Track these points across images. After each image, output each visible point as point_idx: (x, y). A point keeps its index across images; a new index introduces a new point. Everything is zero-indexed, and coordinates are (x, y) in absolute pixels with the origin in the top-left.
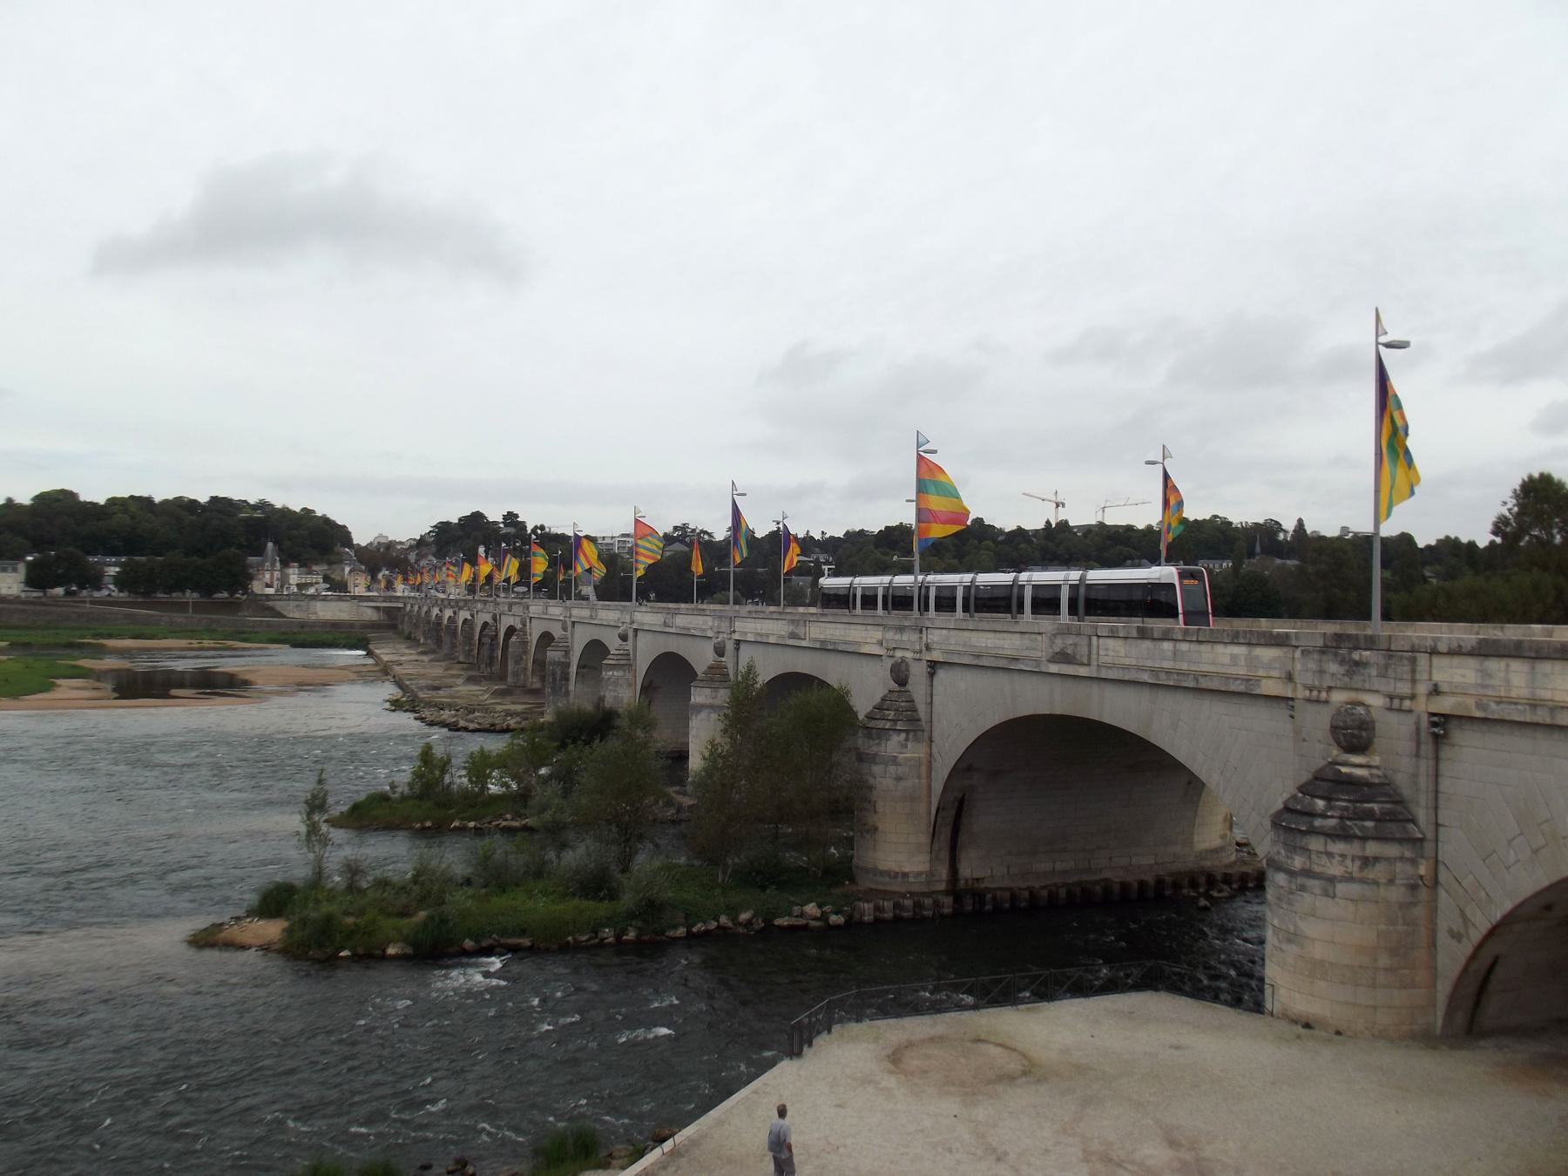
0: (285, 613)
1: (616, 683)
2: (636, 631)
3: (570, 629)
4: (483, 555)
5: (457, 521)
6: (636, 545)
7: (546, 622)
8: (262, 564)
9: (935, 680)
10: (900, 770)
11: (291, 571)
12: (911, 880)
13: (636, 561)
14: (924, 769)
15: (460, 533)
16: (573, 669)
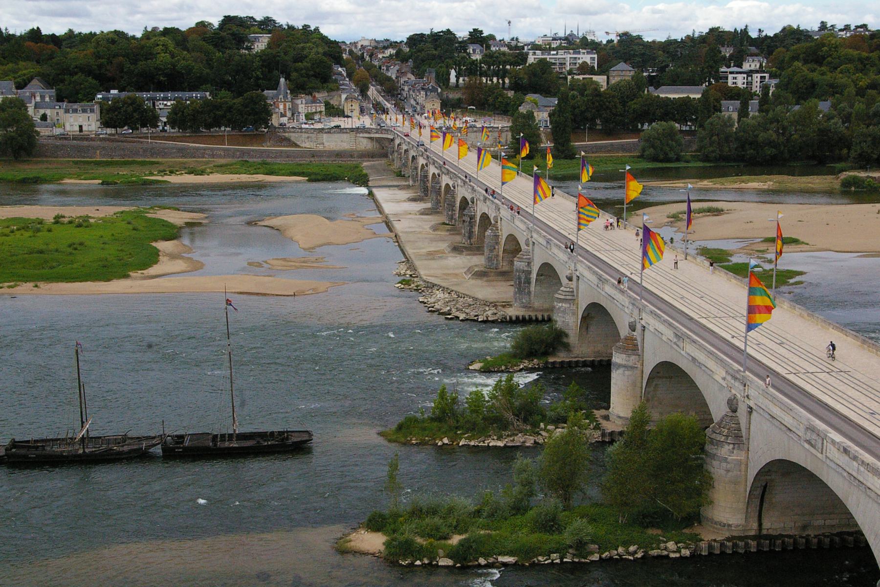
0: (298, 143)
8: (277, 96)
9: (752, 415)
10: (729, 466)
11: (299, 102)
12: (733, 528)
14: (743, 467)
16: (534, 276)
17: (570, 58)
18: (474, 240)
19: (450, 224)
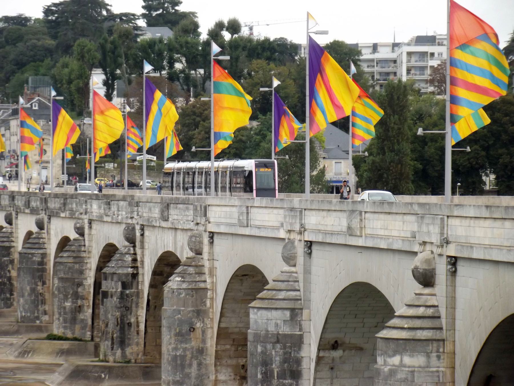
1: (107, 286)
2: (453, 261)
3: (300, 259)
4: (102, 91)
5: (40, 15)
6: (453, 63)
7: (248, 243)
13: (454, 100)
15: (50, 42)
17: (409, 54)
18: (135, 348)
19: (69, 335)
